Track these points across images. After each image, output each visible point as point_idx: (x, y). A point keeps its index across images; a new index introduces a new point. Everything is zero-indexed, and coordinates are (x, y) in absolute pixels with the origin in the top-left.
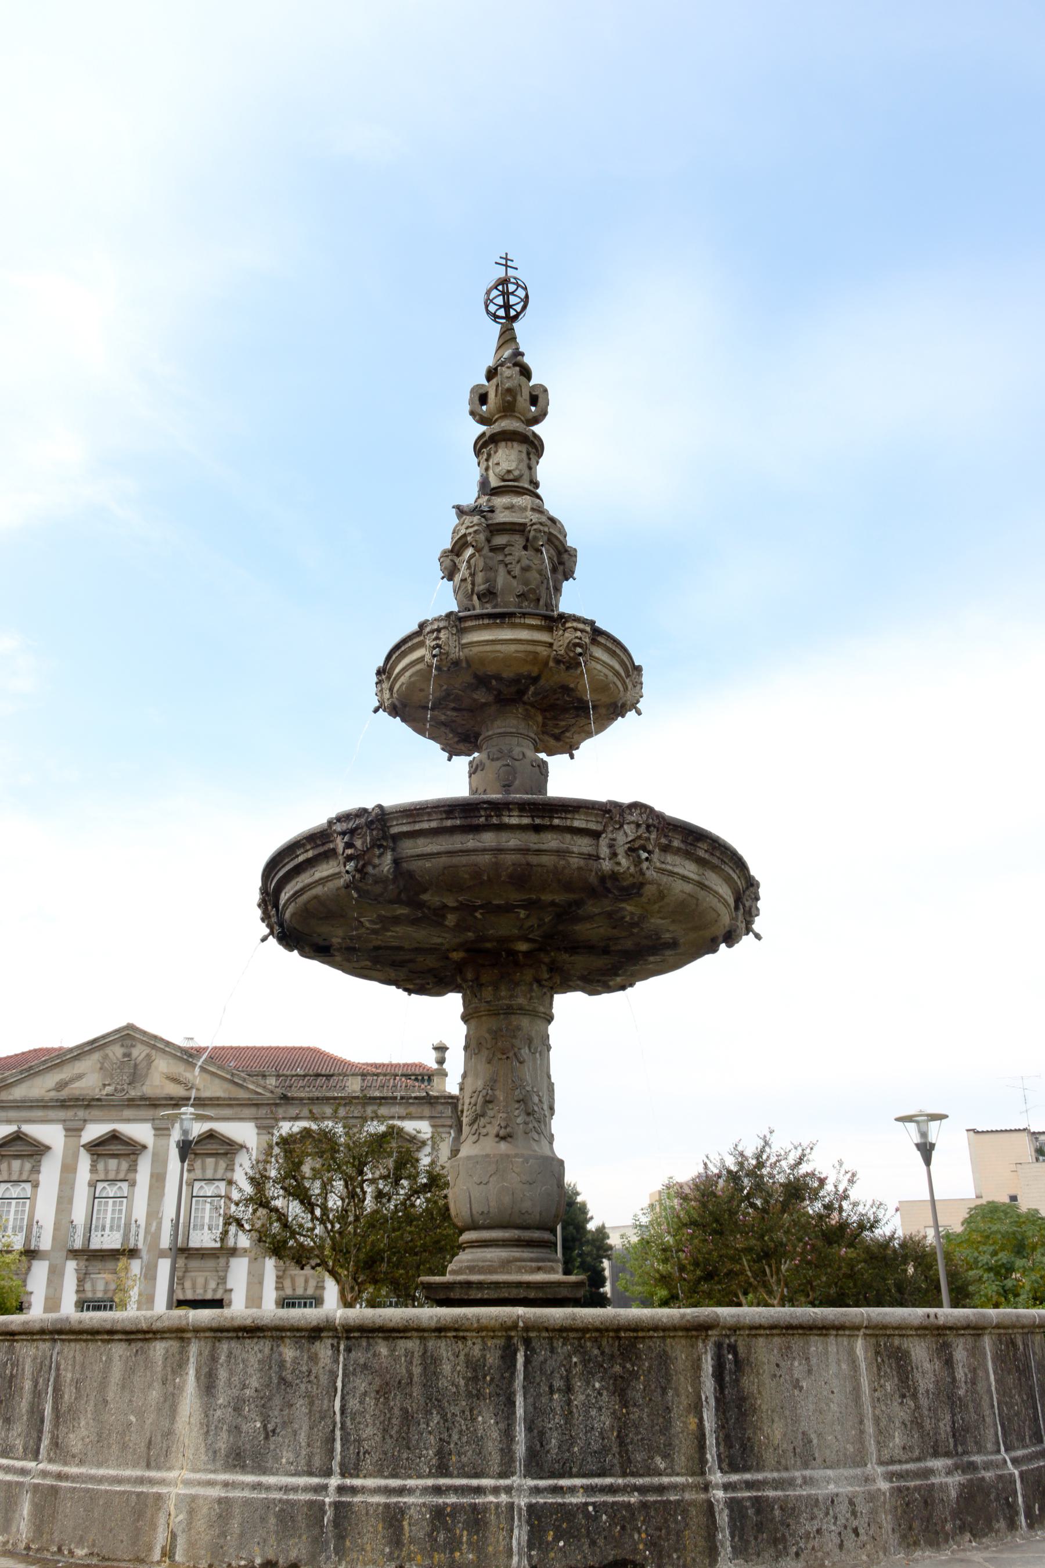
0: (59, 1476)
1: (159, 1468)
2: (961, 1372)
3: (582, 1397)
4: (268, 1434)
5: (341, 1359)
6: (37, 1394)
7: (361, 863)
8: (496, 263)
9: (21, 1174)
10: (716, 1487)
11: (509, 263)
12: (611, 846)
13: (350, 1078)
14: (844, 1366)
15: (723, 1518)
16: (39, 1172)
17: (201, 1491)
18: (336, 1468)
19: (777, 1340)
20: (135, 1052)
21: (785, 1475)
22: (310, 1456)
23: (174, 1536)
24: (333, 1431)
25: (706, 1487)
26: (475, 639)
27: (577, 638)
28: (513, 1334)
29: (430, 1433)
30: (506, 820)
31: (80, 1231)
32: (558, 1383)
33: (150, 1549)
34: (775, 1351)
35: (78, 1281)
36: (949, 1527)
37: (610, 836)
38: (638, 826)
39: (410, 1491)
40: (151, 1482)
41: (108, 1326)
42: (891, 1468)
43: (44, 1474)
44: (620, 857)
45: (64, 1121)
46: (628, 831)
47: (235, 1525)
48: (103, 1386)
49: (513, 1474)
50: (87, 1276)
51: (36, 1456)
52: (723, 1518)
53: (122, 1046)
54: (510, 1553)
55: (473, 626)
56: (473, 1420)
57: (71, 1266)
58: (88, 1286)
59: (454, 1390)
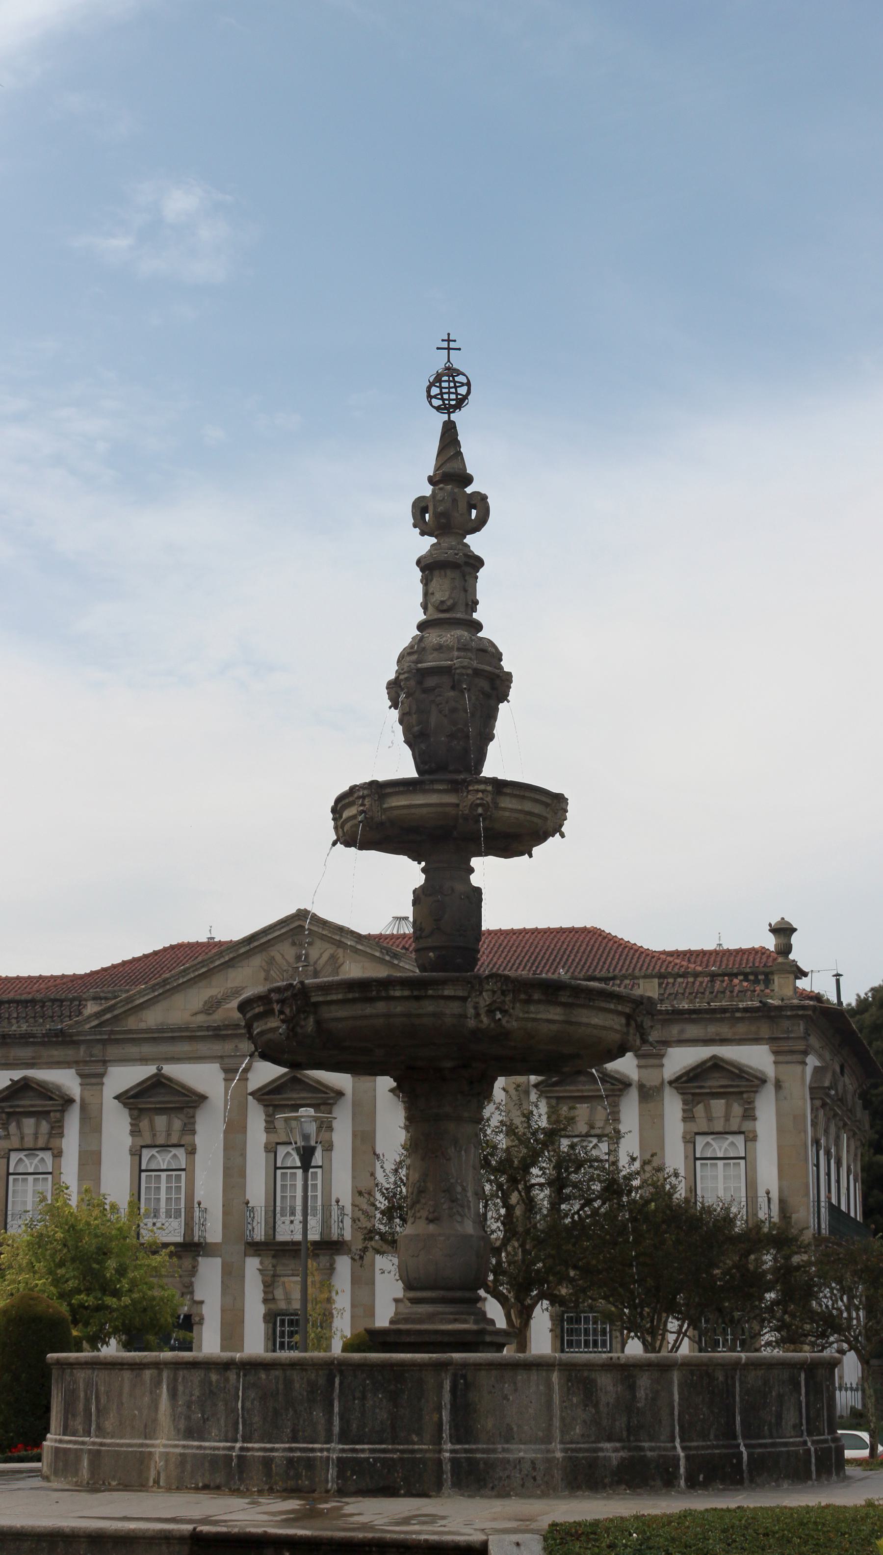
0: (101, 1444)
1: (151, 1439)
2: (642, 1392)
3: (371, 1403)
4: (205, 1420)
5: (241, 1380)
6: (88, 1400)
7: (291, 1025)
8: (438, 348)
9: (169, 1135)
10: (446, 1451)
11: (452, 345)
12: (476, 1008)
13: (641, 981)
14: (541, 1388)
15: (447, 1467)
16: (193, 1132)
17: (172, 1450)
18: (239, 1436)
19: (494, 1373)
20: (314, 953)
21: (491, 1446)
22: (227, 1432)
23: (159, 1473)
24: (238, 1419)
25: (440, 1451)
26: (394, 804)
27: (478, 799)
28: (332, 1367)
29: (288, 1420)
30: (392, 993)
31: (260, 1216)
32: (358, 1394)
33: (148, 1479)
34: (493, 1378)
35: (265, 1286)
36: (607, 1480)
37: (474, 1000)
38: (494, 992)
39: (276, 1450)
40: (147, 1446)
41: (120, 1361)
42: (568, 1446)
43: (94, 1443)
44: (482, 1016)
45: (221, 1057)
46: (486, 997)
47: (188, 1467)
48: (120, 1394)
49: (332, 1442)
50: (277, 1279)
51: (89, 1436)
52: (447, 1467)
53: (294, 944)
54: (327, 1482)
55: (392, 793)
56: (311, 1413)
57: (252, 1265)
58: (279, 1293)
59: (301, 1397)
